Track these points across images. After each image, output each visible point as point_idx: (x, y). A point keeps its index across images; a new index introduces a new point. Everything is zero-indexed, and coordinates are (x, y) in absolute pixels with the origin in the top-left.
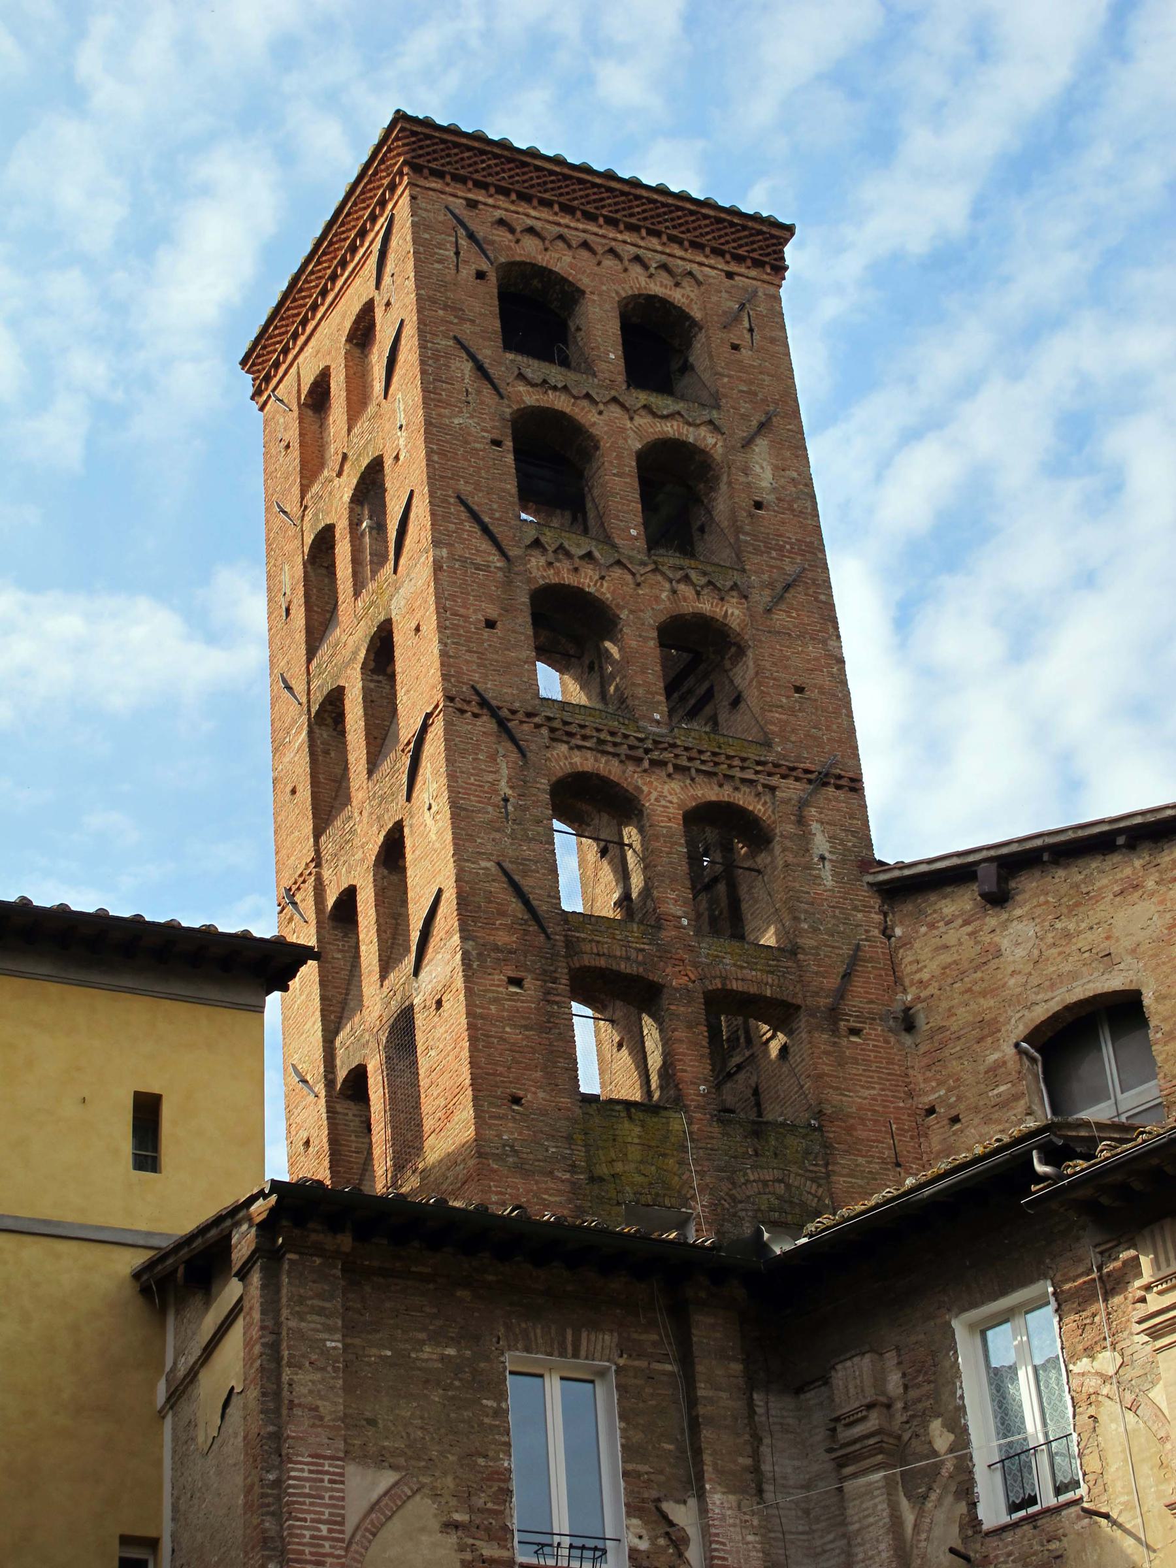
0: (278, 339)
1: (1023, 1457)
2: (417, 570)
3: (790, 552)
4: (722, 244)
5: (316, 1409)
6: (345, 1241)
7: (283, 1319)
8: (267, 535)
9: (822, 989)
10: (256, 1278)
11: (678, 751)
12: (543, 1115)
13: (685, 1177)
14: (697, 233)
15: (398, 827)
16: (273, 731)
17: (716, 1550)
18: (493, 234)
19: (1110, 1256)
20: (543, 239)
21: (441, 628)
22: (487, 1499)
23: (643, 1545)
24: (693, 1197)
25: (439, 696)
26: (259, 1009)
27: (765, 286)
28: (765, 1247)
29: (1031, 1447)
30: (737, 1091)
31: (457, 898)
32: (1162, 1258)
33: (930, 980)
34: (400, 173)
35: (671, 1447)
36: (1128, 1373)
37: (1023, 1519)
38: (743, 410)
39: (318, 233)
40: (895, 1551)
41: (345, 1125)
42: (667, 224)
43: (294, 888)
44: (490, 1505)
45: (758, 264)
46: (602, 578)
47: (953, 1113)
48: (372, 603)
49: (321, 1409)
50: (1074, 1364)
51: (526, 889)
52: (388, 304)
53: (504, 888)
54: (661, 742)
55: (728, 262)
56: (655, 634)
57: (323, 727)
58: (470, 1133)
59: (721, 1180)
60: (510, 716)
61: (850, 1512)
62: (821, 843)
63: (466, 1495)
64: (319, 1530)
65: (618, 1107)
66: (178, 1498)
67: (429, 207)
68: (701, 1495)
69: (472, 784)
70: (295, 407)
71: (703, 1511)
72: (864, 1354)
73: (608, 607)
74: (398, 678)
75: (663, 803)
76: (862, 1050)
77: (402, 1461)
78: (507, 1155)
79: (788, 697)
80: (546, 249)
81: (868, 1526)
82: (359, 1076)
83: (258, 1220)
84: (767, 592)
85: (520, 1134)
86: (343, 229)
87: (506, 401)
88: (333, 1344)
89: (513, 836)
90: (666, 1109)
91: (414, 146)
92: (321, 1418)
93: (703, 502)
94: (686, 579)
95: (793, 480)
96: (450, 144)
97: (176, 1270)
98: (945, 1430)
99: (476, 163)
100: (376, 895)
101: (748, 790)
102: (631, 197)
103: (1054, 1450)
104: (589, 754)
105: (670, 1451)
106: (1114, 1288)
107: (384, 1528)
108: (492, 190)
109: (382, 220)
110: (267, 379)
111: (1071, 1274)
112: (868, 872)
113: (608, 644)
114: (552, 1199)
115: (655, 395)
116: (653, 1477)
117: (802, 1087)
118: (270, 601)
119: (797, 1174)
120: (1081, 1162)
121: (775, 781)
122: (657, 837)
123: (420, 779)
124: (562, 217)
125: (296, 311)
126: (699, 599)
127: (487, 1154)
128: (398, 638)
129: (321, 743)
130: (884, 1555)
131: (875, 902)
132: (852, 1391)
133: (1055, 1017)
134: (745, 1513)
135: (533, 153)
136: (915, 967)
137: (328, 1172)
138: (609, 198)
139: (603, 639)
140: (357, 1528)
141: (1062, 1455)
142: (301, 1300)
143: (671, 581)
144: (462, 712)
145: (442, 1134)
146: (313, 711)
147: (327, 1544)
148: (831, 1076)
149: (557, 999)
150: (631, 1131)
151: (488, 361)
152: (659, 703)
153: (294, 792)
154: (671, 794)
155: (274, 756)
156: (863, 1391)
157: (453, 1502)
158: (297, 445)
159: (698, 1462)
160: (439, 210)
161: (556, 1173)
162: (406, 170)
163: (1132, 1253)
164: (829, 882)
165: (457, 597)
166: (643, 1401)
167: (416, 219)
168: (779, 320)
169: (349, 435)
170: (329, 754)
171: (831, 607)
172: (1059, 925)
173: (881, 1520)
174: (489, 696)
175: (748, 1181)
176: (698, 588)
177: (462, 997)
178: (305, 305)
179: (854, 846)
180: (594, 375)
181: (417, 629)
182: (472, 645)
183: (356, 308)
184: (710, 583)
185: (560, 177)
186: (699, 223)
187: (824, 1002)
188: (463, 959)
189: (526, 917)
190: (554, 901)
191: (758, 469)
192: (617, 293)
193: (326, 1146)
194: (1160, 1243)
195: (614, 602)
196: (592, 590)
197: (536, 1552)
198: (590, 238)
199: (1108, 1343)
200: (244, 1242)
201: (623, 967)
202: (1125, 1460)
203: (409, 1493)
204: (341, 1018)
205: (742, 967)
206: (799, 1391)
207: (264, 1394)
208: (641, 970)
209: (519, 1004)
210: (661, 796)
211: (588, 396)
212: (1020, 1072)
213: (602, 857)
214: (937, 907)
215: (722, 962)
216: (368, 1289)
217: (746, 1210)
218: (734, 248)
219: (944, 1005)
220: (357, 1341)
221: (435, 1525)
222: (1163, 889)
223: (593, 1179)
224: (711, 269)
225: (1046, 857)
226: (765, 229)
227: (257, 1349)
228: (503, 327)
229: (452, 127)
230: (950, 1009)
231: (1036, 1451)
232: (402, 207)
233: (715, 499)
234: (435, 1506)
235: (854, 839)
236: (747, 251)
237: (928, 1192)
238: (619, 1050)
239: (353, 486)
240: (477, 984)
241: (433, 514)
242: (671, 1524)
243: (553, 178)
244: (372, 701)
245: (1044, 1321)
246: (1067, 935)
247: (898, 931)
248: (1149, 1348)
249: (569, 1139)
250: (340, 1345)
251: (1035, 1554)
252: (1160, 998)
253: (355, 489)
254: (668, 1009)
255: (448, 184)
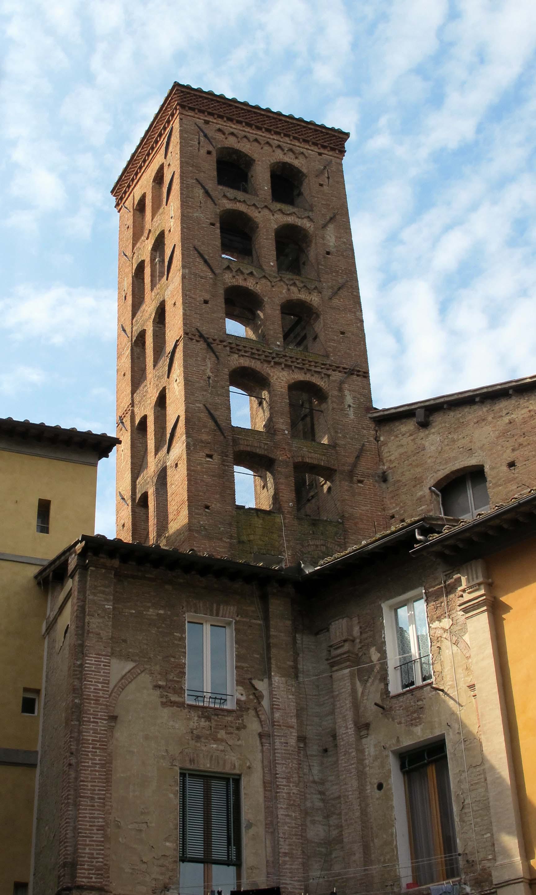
0: (126, 181)
1: (409, 664)
2: (175, 279)
3: (341, 273)
4: (317, 141)
5: (99, 634)
6: (116, 563)
7: (87, 595)
8: (119, 265)
9: (346, 463)
10: (77, 578)
11: (287, 358)
12: (219, 514)
13: (281, 542)
14: (306, 136)
15: (164, 389)
16: (118, 349)
17: (275, 701)
18: (215, 135)
19: (449, 577)
20: (237, 137)
21: (184, 303)
22: (174, 676)
23: (243, 698)
24: (284, 551)
25: (181, 333)
26: (96, 465)
27: (335, 159)
28: (301, 570)
29: (413, 659)
30: (309, 508)
31: (185, 419)
32: (470, 578)
33: (395, 460)
34: (176, 109)
35: (258, 656)
36: (456, 628)
37: (408, 691)
38: (323, 212)
39: (142, 135)
40: (353, 704)
41: (140, 518)
42: (293, 132)
43: (123, 416)
44: (175, 678)
45: (333, 149)
46: (257, 283)
47: (402, 518)
48: (158, 293)
49: (101, 634)
50: (432, 624)
51: (216, 416)
52: (169, 165)
53: (206, 416)
54: (279, 355)
55: (319, 149)
56: (279, 308)
57: (138, 347)
58: (186, 521)
59: (298, 544)
60: (212, 342)
61: (334, 686)
62: (349, 400)
63: (165, 674)
64: (97, 686)
65: (252, 511)
66: (48, 672)
67: (188, 123)
68: (270, 678)
69: (194, 371)
70: (131, 210)
71: (270, 684)
72: (344, 618)
73: (259, 295)
74: (166, 325)
75: (279, 380)
76: (363, 489)
77: (137, 658)
78: (202, 530)
79: (337, 336)
80: (239, 142)
81: (342, 693)
82: (145, 496)
83: (78, 552)
84: (331, 290)
85: (208, 522)
86: (153, 133)
87: (218, 207)
88: (108, 607)
89: (211, 393)
90: (274, 513)
91: (182, 97)
92: (102, 638)
93: (304, 252)
94: (294, 284)
95: (344, 242)
96: (198, 97)
97: (49, 575)
98: (377, 652)
99: (209, 105)
100: (155, 419)
101: (317, 376)
102: (277, 120)
103: (423, 662)
104: (247, 359)
105: (257, 658)
106: (450, 591)
107: (128, 687)
108: (216, 116)
109: (168, 129)
110: (121, 199)
111: (433, 584)
112: (369, 413)
113: (259, 312)
114: (221, 550)
115: (284, 205)
116: (249, 669)
117: (336, 505)
118: (119, 293)
119: (332, 543)
120: (436, 534)
121: (330, 372)
122: (276, 395)
123: (173, 370)
124: (246, 128)
125: (133, 170)
126: (299, 293)
127: (193, 530)
128: (167, 308)
129: (137, 354)
130: (348, 706)
131: (372, 425)
132: (338, 634)
133: (447, 477)
134: (289, 686)
135: (234, 100)
136: (388, 454)
137: (131, 538)
138: (267, 120)
139: (257, 310)
140: (115, 686)
141: (426, 664)
142: (96, 587)
143: (287, 285)
144: (192, 339)
145: (176, 521)
146: (133, 340)
147: (101, 692)
148: (349, 500)
149: (228, 464)
150: (258, 522)
151: (210, 189)
152: (280, 337)
153: (124, 375)
154: (283, 377)
155: (118, 360)
156: (342, 634)
157: (159, 677)
158: (132, 227)
159: (269, 663)
160: (192, 125)
161: (223, 539)
162: (178, 107)
163: (459, 575)
164: (352, 416)
165: (192, 290)
166: (247, 636)
167: (181, 128)
168: (341, 174)
169: (152, 221)
170: (139, 359)
171: (359, 297)
172: (450, 437)
173: (347, 690)
174: (204, 333)
175: (309, 545)
176: (299, 288)
177: (185, 462)
178: (137, 167)
179: (364, 401)
180: (258, 196)
181: (175, 304)
182: (197, 311)
183: (157, 167)
184: (305, 286)
185: (246, 111)
186: (307, 131)
187: (347, 468)
188: (187, 446)
189: (216, 428)
190: (228, 422)
191: (328, 237)
192: (269, 161)
193: (131, 526)
194: (470, 571)
195: (262, 294)
196: (252, 288)
197: (195, 700)
198: (258, 137)
199: (447, 615)
200: (73, 562)
201: (258, 451)
202: (451, 666)
203: (140, 672)
204: (139, 472)
205: (310, 452)
206: (317, 634)
207: (77, 627)
208: (266, 452)
209: (211, 466)
210: (279, 378)
211: (254, 205)
212: (431, 500)
213: (259, 406)
214: (398, 428)
215: (302, 450)
216: (126, 584)
217: (307, 557)
218: (322, 142)
219: (400, 471)
220: (120, 606)
221: (150, 686)
222: (495, 421)
223: (240, 542)
224: (312, 151)
225: (445, 406)
226: (336, 134)
227: (76, 608)
228: (218, 175)
229: (199, 89)
230: (402, 473)
231: (415, 662)
232: (176, 124)
233: (310, 251)
234: (151, 678)
235: (365, 399)
236: (328, 144)
237: (371, 547)
238: (263, 489)
239: (152, 243)
240: (192, 456)
241: (183, 254)
242: (256, 689)
243: (243, 111)
244: (157, 336)
245: (421, 606)
246: (454, 441)
247: (382, 439)
248: (464, 617)
249: (230, 524)
250: (111, 607)
251: (412, 706)
252: (492, 468)
253: (153, 245)
254: (277, 470)
255: (196, 114)
